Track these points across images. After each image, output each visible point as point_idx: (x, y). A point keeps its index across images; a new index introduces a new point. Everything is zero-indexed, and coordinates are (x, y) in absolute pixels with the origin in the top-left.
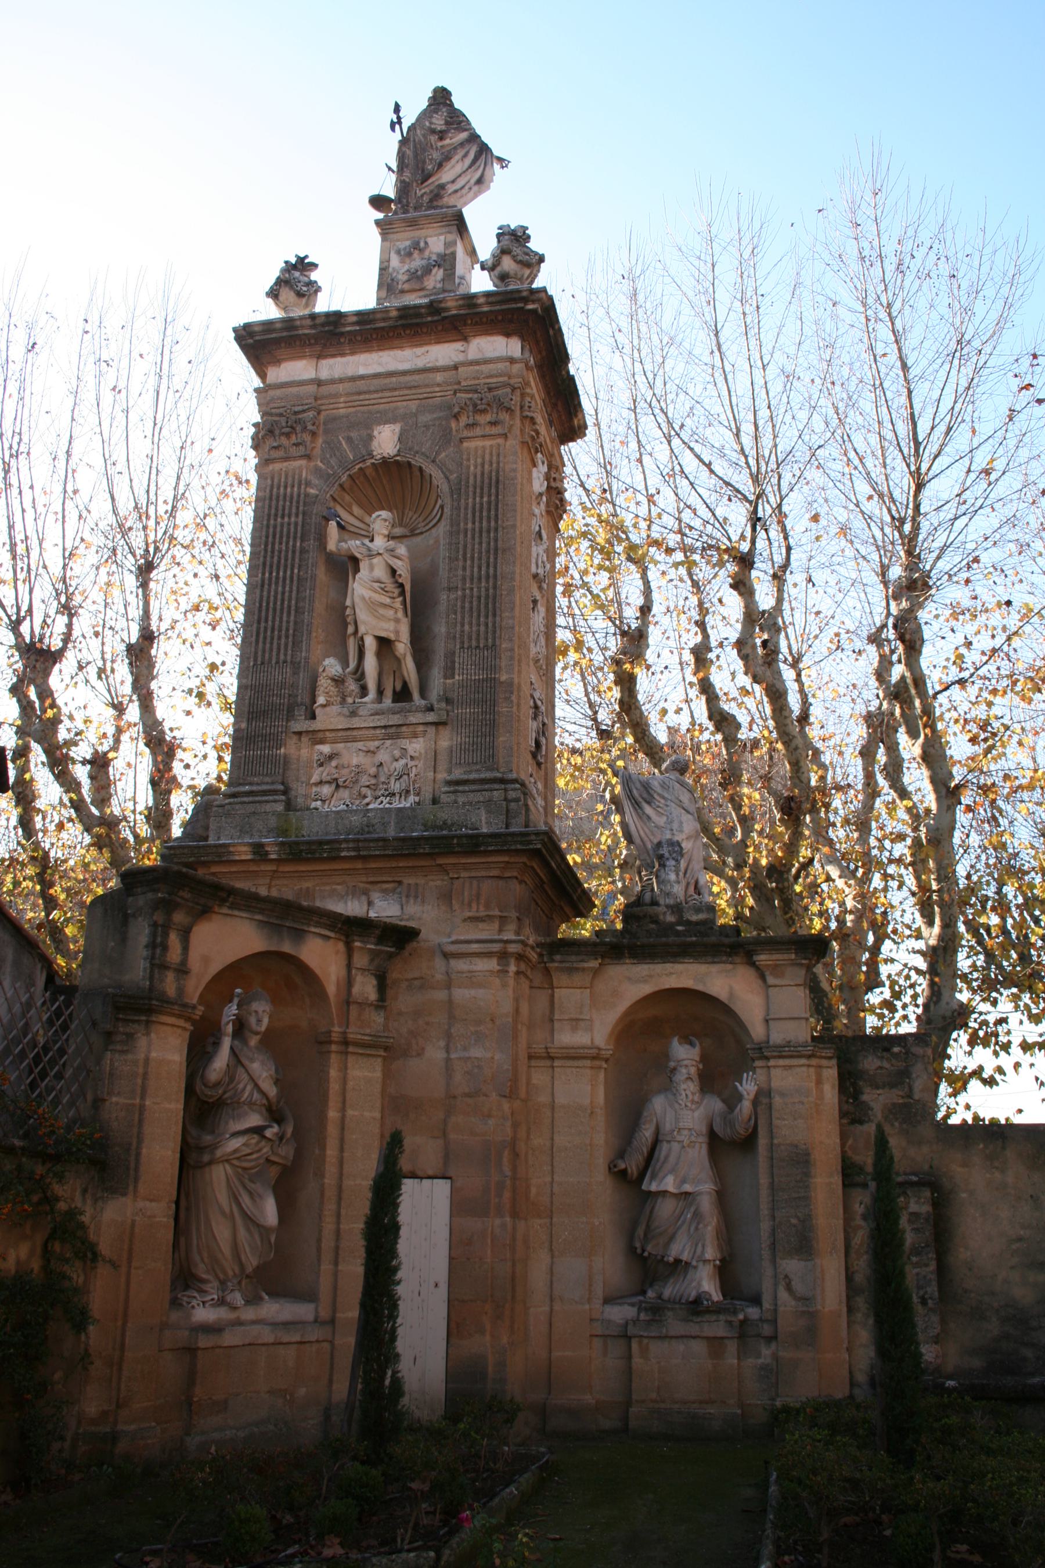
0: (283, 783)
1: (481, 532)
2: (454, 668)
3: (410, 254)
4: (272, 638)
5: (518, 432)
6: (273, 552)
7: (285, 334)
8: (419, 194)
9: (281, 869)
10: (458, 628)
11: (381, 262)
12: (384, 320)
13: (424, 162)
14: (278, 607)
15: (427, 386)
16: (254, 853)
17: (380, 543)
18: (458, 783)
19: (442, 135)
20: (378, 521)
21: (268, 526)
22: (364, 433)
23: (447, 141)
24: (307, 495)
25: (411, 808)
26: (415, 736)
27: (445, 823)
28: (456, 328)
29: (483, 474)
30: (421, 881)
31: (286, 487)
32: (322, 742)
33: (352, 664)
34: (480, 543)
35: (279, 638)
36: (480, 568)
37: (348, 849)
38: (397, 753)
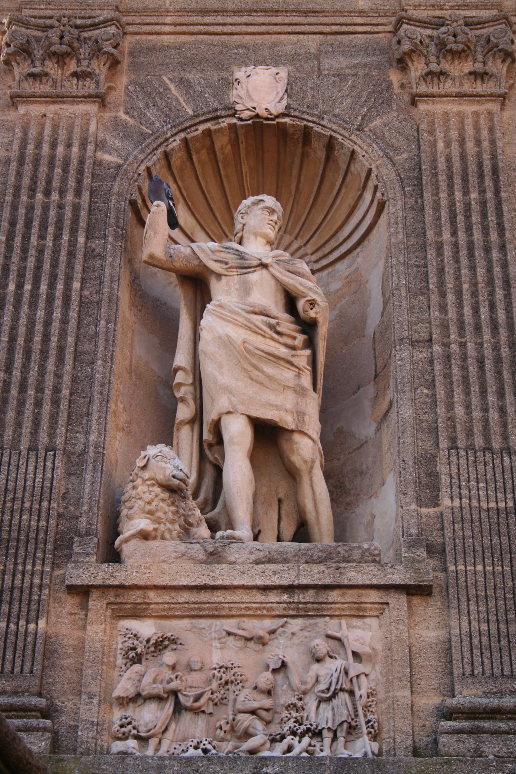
1: (471, 248)
6: (25, 250)
10: (441, 409)
18: (473, 713)
20: (257, 210)
22: (214, 76)
24: (98, 163)
26: (359, 613)
29: (463, 157)
31: (53, 146)
32: (137, 613)
34: (473, 268)
35: (38, 403)
36: (476, 311)
38: (322, 646)
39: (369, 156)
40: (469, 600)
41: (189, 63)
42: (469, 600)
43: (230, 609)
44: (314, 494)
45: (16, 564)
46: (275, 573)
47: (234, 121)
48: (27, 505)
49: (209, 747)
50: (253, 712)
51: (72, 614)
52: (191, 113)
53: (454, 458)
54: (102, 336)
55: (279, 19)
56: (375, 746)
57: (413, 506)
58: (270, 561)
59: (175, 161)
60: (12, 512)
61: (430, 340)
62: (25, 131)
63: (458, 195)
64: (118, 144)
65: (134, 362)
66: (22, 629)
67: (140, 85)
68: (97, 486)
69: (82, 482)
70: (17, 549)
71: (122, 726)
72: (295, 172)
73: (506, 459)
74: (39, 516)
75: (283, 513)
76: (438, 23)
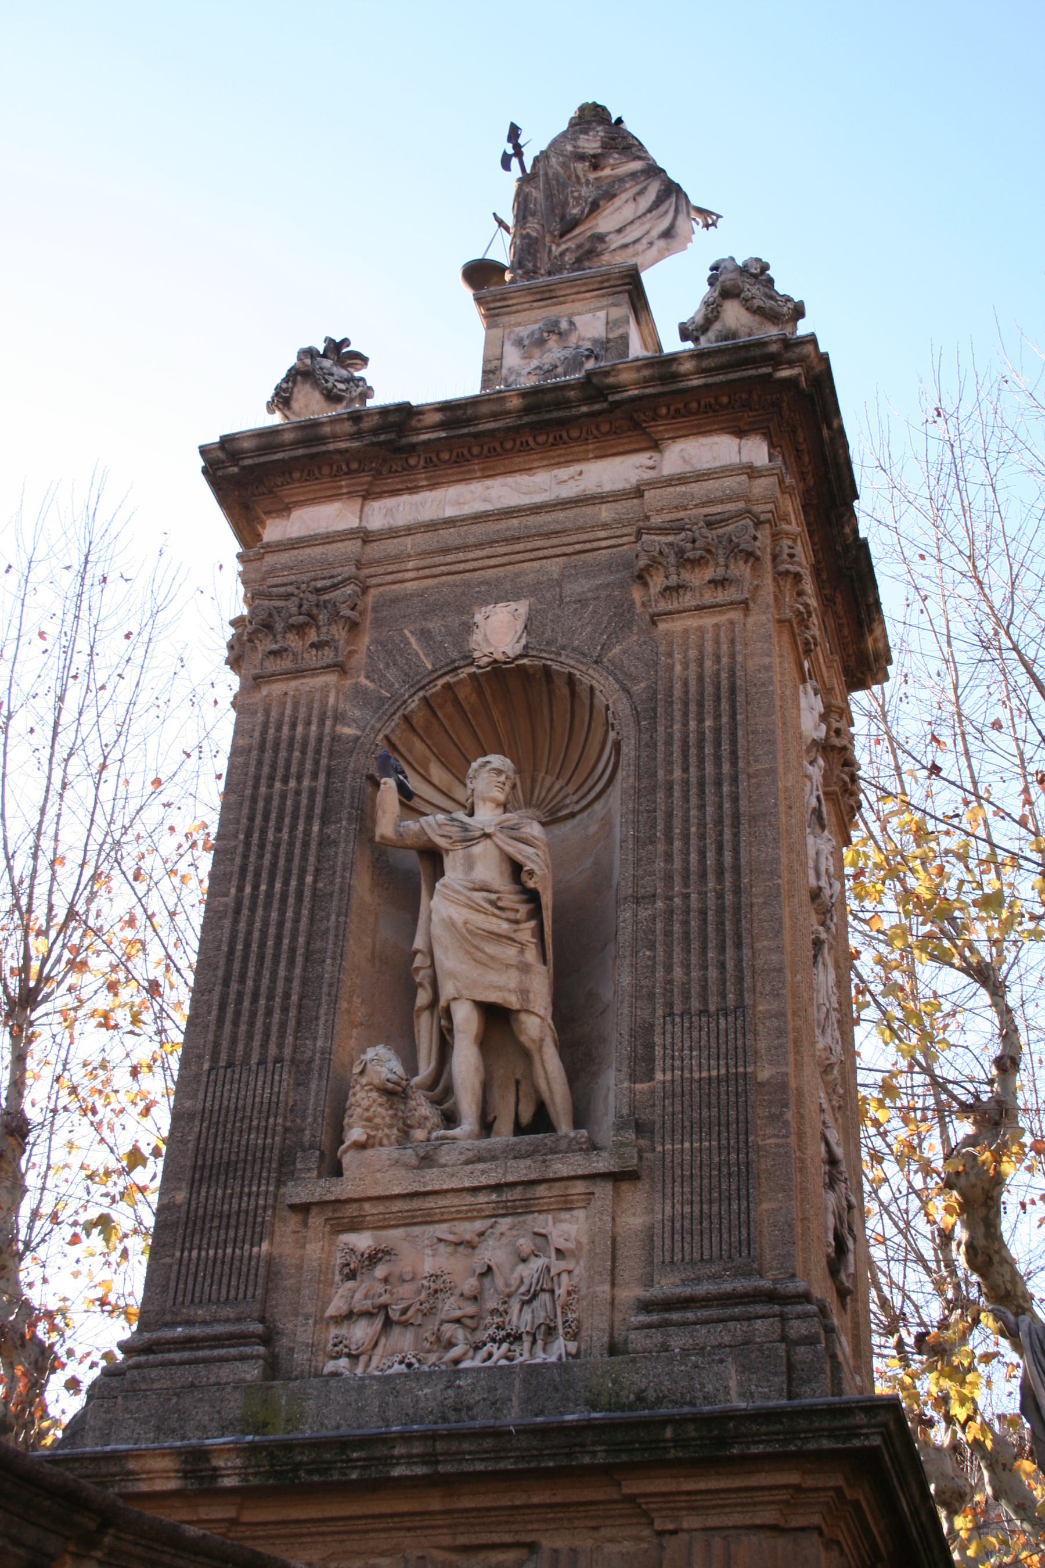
0: (262, 1320)
1: (701, 784)
2: (652, 1060)
3: (541, 342)
4: (253, 1015)
5: (771, 600)
6: (262, 846)
7: (300, 452)
8: (556, 250)
9: (248, 1516)
10: (660, 973)
11: (486, 361)
12: (495, 416)
13: (565, 204)
14: (269, 951)
15: (581, 529)
16: (186, 1475)
17: (486, 816)
18: (669, 1304)
19: (596, 162)
20: (484, 774)
21: (254, 800)
22: (454, 621)
23: (607, 172)
24: (336, 738)
25: (559, 1364)
26: (566, 1205)
27: (641, 1398)
28: (636, 426)
29: (701, 678)
30: (585, 1542)
31: (293, 726)
32: (355, 1226)
33: (426, 1069)
34: (702, 807)
35: (269, 1013)
36: (702, 854)
37: (410, 1459)
38: (525, 1244)
39: (607, 691)
40: (674, 1181)
41: (430, 610)
42: (674, 1181)
43: (442, 1214)
44: (546, 1072)
45: (242, 1186)
46: (483, 1172)
47: (473, 669)
48: (255, 1123)
49: (413, 1360)
50: (458, 1321)
51: (295, 1232)
52: (430, 667)
53: (669, 1027)
54: (332, 932)
55: (520, 547)
56: (572, 1347)
57: (626, 1084)
58: (480, 1159)
59: (418, 721)
60: (241, 1132)
61: (654, 896)
62: (267, 713)
63: (693, 724)
64: (357, 713)
65: (378, 947)
66: (246, 1254)
67: (381, 643)
68: (322, 1095)
69: (308, 1093)
70: (244, 1170)
71: (335, 1345)
72: (546, 711)
73: (722, 1021)
74: (266, 1134)
75: (521, 1094)
76: (676, 528)
